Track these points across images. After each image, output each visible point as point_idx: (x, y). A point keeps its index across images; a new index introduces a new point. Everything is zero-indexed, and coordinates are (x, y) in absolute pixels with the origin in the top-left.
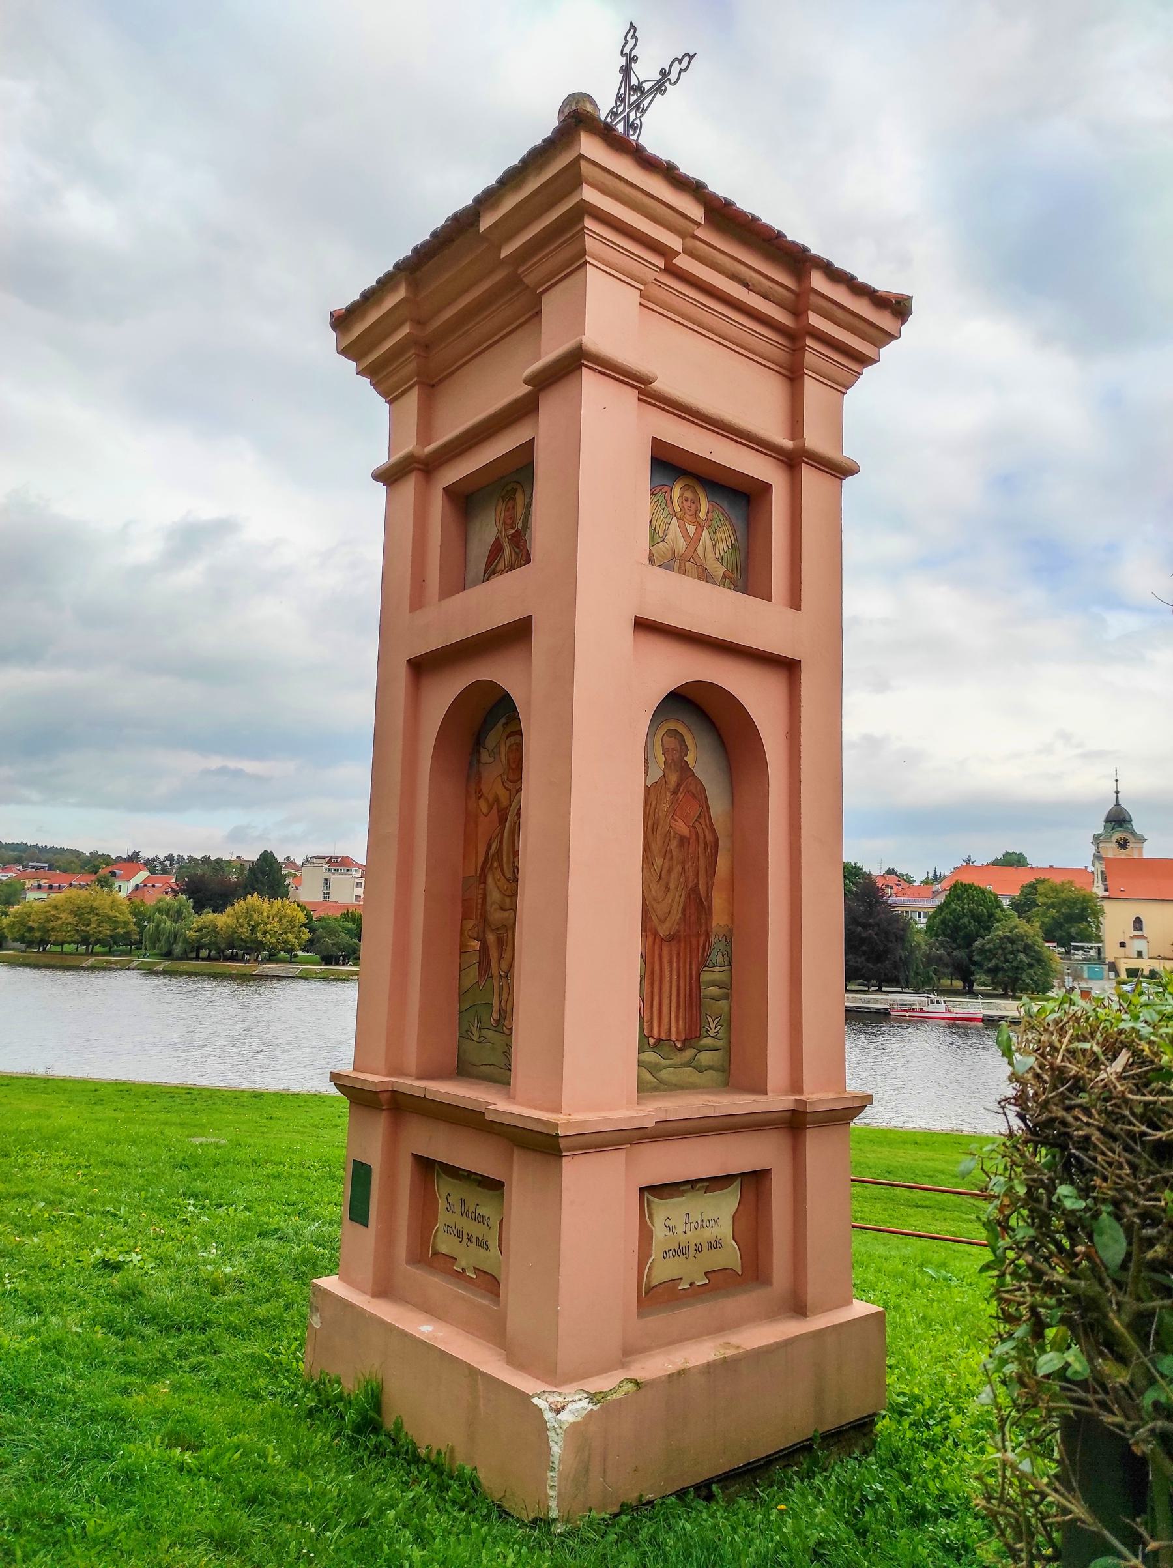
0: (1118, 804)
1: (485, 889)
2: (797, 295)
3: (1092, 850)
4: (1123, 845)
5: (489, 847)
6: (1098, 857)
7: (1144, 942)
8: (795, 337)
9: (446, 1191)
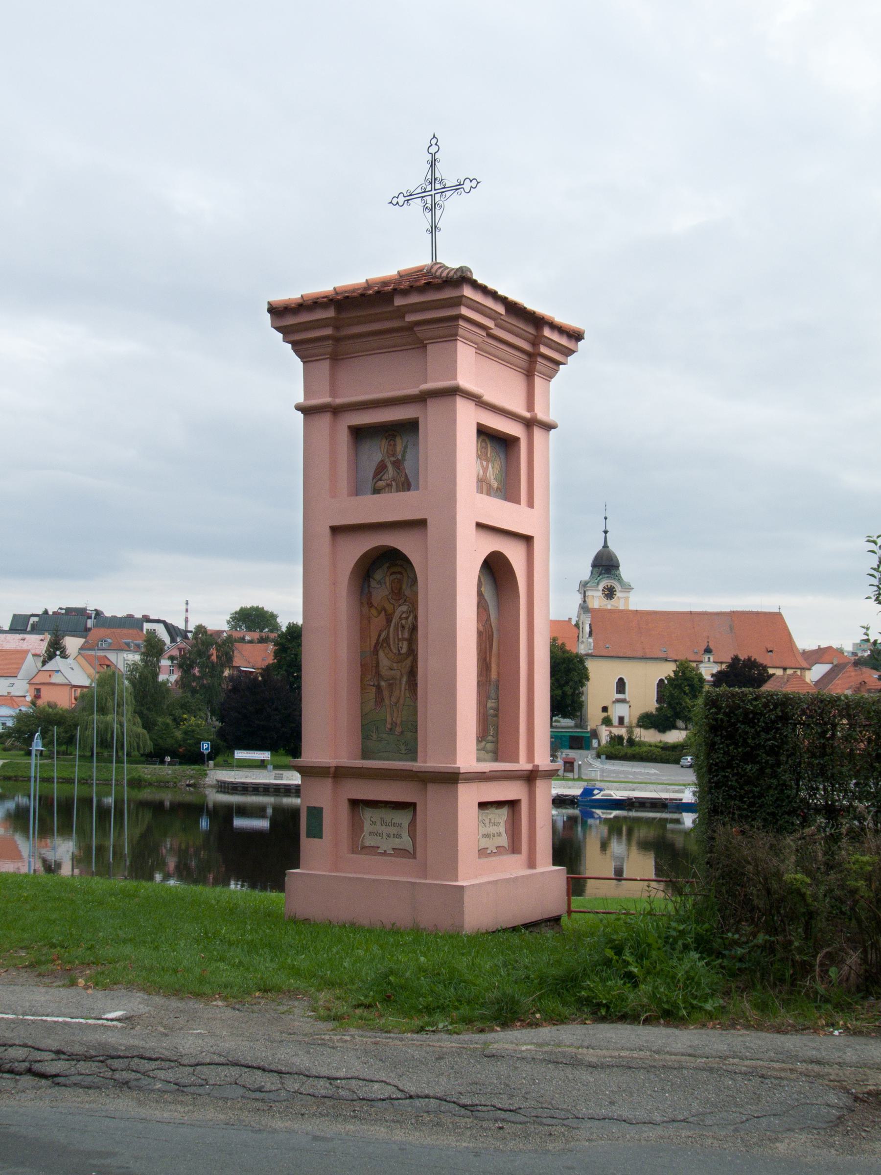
0: (605, 546)
1: (377, 659)
2: (536, 337)
3: (579, 599)
4: (610, 593)
5: (379, 636)
6: (584, 607)
7: (626, 706)
8: (532, 357)
9: (368, 815)
